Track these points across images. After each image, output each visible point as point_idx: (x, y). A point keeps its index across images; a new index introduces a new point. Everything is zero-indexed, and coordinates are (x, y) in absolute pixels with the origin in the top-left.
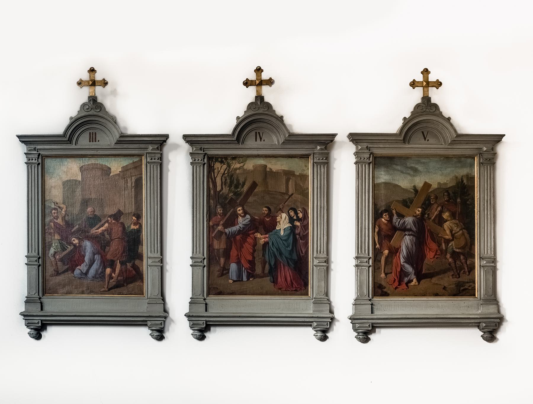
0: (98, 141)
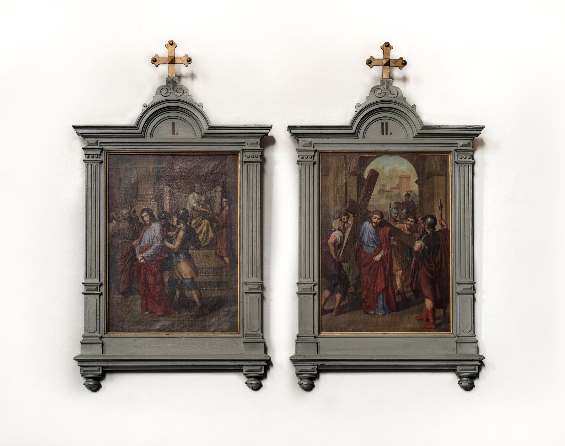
0: (391, 134)
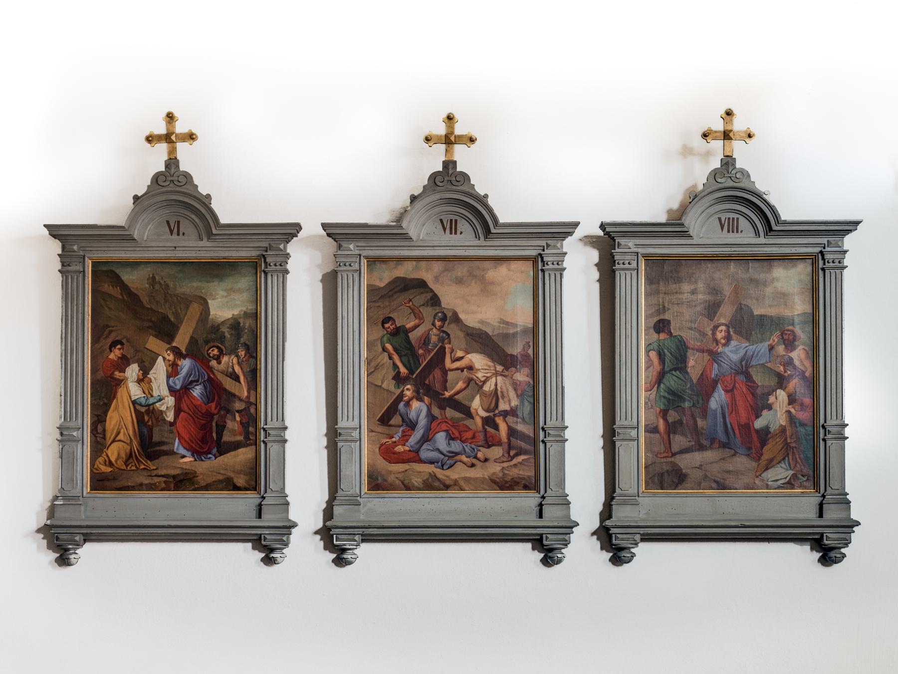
0: (741, 232)
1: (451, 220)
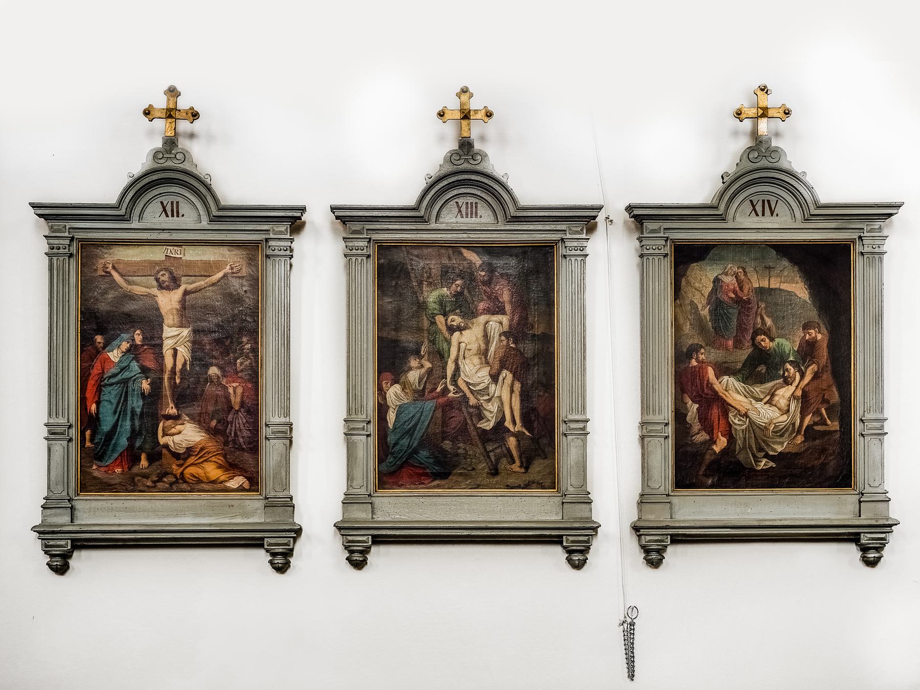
0: (183, 216)
1: (172, 203)
